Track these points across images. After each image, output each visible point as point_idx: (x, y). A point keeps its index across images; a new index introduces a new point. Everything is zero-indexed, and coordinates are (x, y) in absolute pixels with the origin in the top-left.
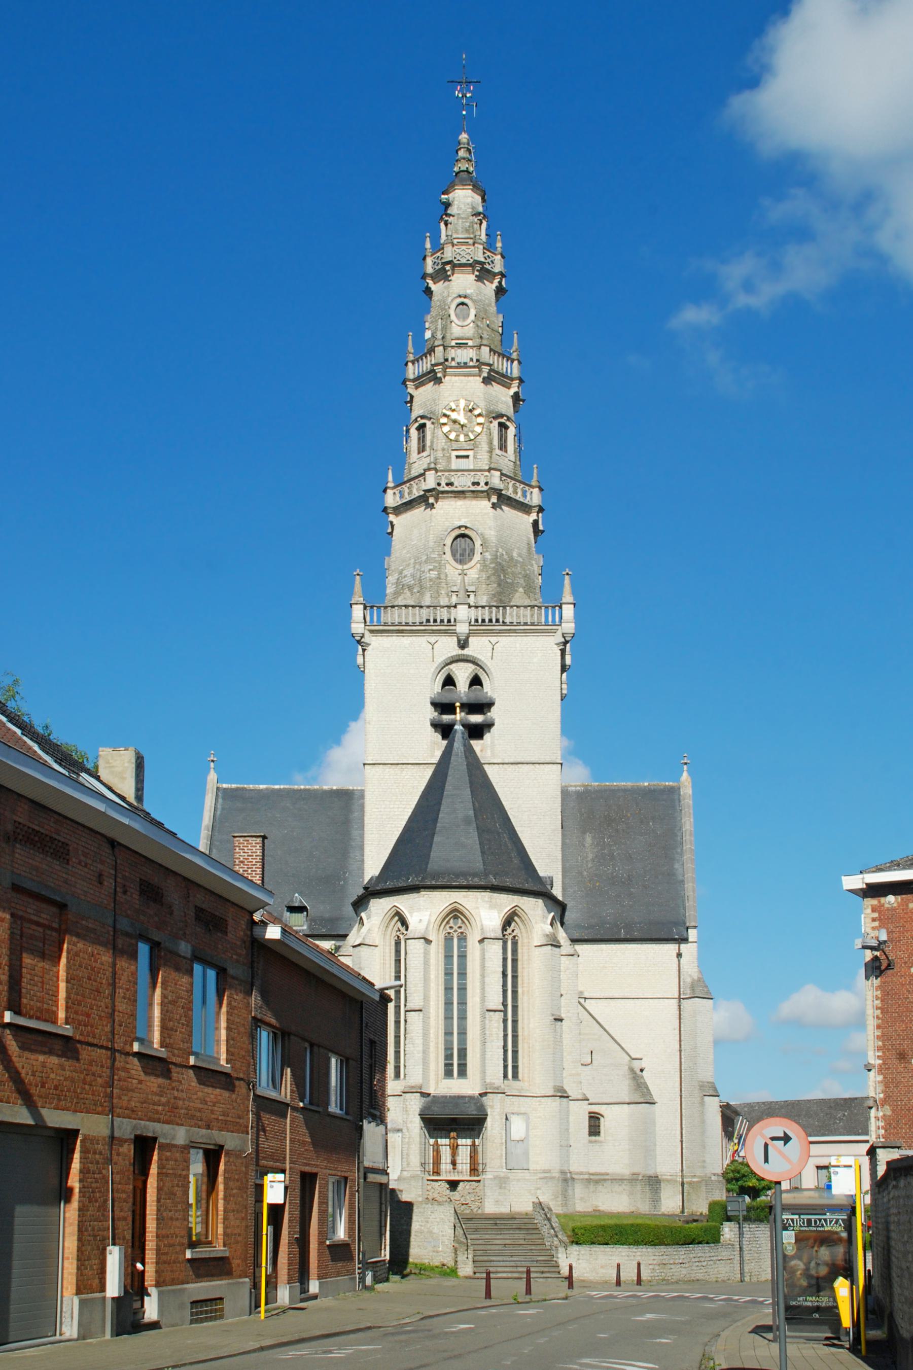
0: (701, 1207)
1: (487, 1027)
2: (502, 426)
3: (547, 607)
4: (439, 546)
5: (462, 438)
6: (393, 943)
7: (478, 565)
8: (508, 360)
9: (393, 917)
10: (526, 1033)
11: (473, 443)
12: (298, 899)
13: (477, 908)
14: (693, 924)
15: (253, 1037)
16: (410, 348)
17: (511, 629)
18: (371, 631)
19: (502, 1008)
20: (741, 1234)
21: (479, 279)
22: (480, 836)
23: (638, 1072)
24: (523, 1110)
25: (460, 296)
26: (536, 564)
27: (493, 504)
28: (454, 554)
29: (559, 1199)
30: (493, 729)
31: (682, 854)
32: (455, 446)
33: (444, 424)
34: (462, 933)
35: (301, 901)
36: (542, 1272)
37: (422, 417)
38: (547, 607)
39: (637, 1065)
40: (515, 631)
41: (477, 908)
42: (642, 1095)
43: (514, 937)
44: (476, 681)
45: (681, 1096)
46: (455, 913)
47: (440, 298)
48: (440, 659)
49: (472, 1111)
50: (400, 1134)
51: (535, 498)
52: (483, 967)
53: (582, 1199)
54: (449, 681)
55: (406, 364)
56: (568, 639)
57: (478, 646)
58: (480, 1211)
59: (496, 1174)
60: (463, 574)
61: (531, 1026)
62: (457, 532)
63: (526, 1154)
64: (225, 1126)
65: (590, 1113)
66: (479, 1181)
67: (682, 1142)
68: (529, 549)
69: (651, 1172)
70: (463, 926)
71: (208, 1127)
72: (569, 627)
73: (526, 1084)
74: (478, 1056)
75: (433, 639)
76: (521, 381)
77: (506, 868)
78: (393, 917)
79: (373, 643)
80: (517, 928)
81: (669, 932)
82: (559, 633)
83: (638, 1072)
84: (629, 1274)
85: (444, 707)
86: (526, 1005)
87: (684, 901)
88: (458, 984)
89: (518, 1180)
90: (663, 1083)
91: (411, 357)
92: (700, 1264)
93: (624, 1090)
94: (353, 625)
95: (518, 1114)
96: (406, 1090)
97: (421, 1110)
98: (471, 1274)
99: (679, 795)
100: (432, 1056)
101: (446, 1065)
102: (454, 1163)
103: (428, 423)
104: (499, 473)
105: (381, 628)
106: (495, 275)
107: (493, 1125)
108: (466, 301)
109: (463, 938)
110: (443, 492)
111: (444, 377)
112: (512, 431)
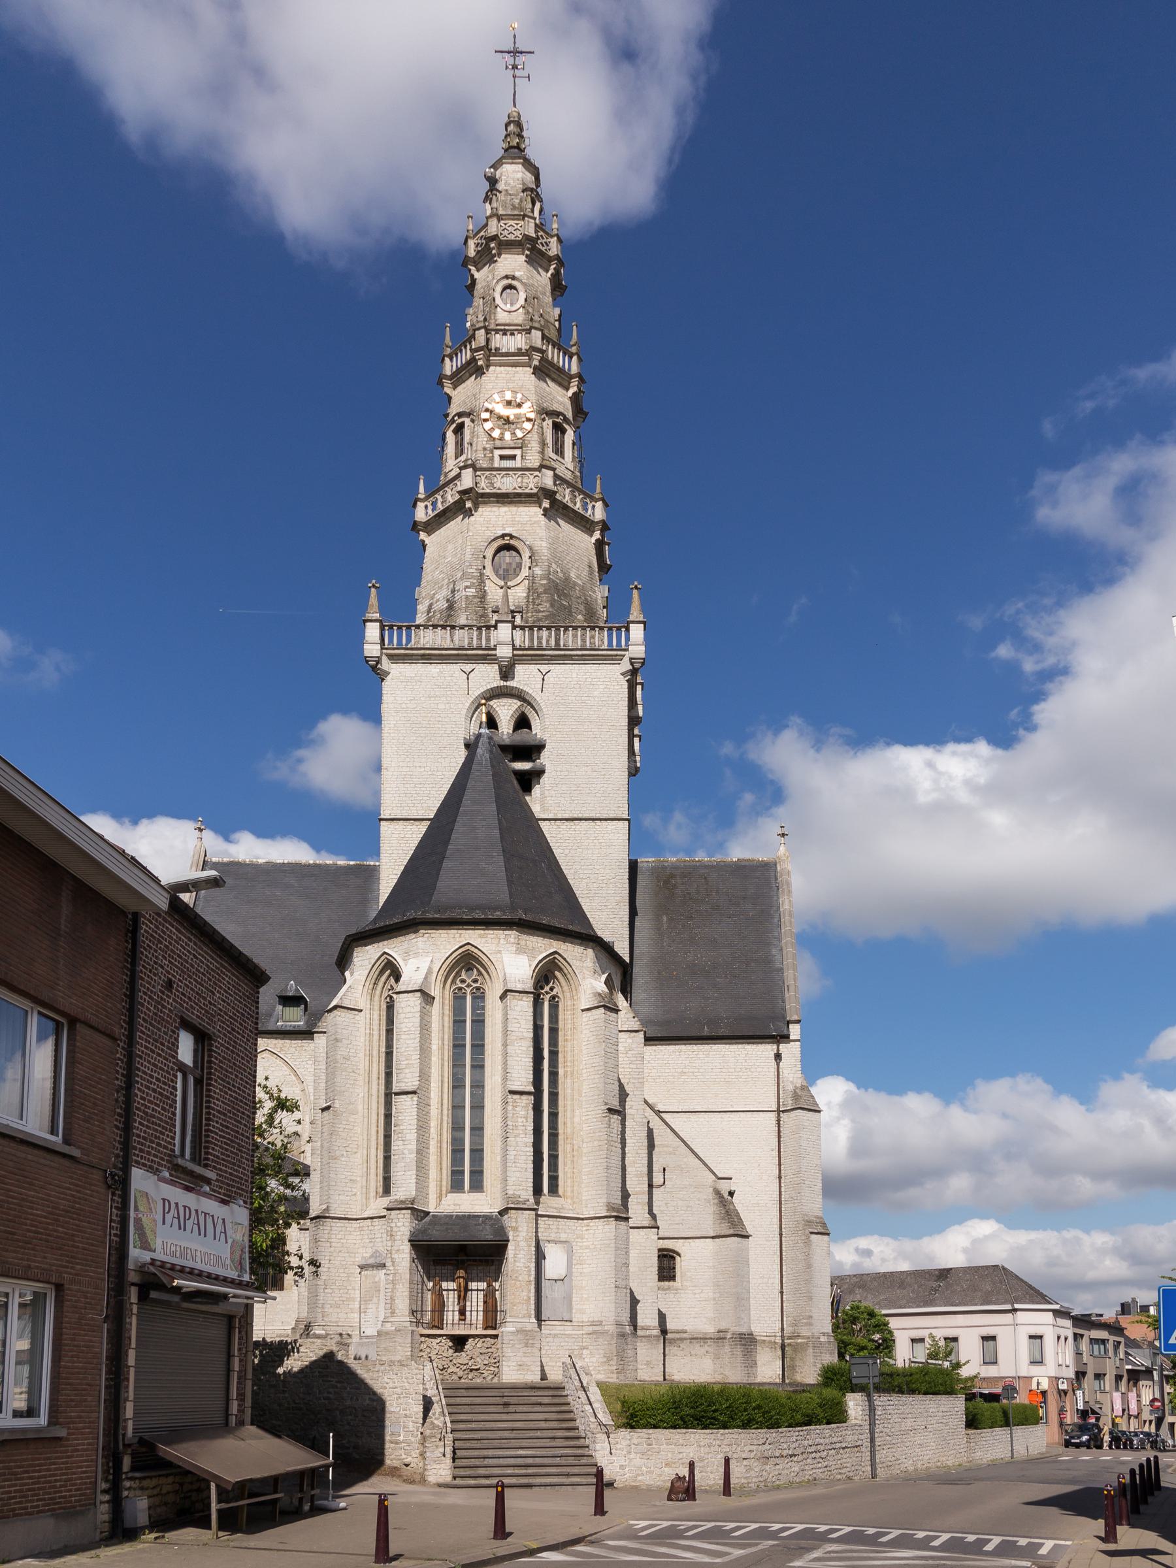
0: (809, 1373)
1: (510, 1115)
2: (558, 429)
3: (610, 629)
4: (477, 559)
5: (508, 436)
6: (384, 1006)
7: (526, 582)
8: (565, 354)
9: (381, 973)
10: (569, 1130)
11: (522, 445)
12: (292, 987)
13: (500, 952)
14: (795, 1017)
16: (448, 340)
17: (564, 657)
18: (392, 658)
19: (532, 1089)
20: (872, 1410)
21: (530, 261)
22: (507, 861)
23: (726, 1195)
24: (563, 1237)
25: (507, 277)
26: (600, 593)
27: (545, 510)
29: (613, 1362)
30: (544, 779)
31: (780, 940)
32: (498, 443)
33: (486, 420)
34: (478, 989)
35: (297, 990)
36: (568, 1475)
37: (460, 415)
38: (610, 629)
39: (724, 1187)
40: (571, 657)
41: (500, 952)
42: (732, 1226)
43: (554, 997)
44: (522, 722)
45: (781, 1235)
46: (467, 961)
47: (484, 284)
50: (381, 1273)
51: (598, 512)
52: (506, 1032)
53: (648, 1363)
55: (443, 360)
56: (637, 666)
57: (526, 677)
58: (496, 1380)
59: (519, 1325)
61: (576, 1120)
62: (500, 542)
63: (568, 1299)
65: (660, 1250)
66: (496, 1336)
67: (782, 1293)
68: (591, 573)
69: (744, 1330)
70: (480, 978)
72: (638, 650)
73: (569, 1201)
74: (499, 1158)
75: (468, 667)
76: (582, 380)
77: (545, 906)
78: (381, 973)
79: (392, 672)
80: (560, 988)
81: (766, 1030)
82: (626, 659)
83: (726, 1195)
84: (709, 1477)
86: (569, 1091)
87: (783, 993)
88: (472, 1059)
89: (555, 1336)
90: (756, 1205)
91: (448, 351)
92: (818, 1455)
93: (707, 1219)
94: (366, 647)
95: (556, 1242)
96: (391, 1206)
97: (412, 1234)
98: (449, 1479)
99: (776, 871)
100: (433, 1159)
101: (453, 1173)
102: (462, 1312)
103: (467, 421)
104: (552, 473)
105: (402, 652)
106: (550, 260)
107: (518, 1258)
108: (514, 283)
109: (479, 996)
110: (483, 495)
111: (488, 366)
112: (570, 436)
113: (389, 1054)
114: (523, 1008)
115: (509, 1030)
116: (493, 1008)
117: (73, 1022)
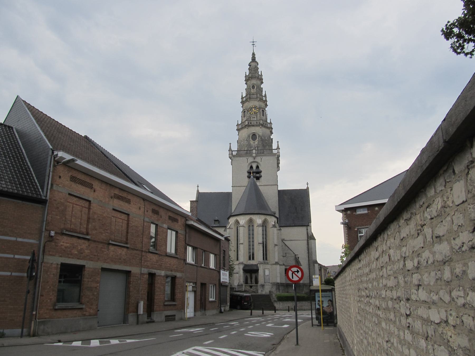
15: (186, 249)
28: (252, 138)
44: (258, 167)
46: (251, 221)
48: (249, 162)
49: (255, 268)
54: (251, 167)
60: (254, 143)
63: (269, 279)
64: (177, 271)
71: (172, 271)
85: (249, 173)
107: (261, 272)
109: (253, 226)
113: (237, 236)
114: (261, 229)
115: (258, 232)
116: (255, 228)
117: (205, 251)
